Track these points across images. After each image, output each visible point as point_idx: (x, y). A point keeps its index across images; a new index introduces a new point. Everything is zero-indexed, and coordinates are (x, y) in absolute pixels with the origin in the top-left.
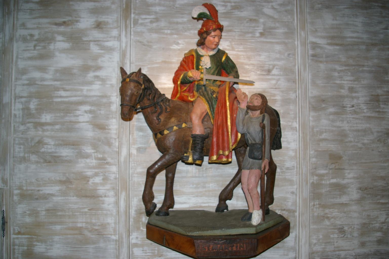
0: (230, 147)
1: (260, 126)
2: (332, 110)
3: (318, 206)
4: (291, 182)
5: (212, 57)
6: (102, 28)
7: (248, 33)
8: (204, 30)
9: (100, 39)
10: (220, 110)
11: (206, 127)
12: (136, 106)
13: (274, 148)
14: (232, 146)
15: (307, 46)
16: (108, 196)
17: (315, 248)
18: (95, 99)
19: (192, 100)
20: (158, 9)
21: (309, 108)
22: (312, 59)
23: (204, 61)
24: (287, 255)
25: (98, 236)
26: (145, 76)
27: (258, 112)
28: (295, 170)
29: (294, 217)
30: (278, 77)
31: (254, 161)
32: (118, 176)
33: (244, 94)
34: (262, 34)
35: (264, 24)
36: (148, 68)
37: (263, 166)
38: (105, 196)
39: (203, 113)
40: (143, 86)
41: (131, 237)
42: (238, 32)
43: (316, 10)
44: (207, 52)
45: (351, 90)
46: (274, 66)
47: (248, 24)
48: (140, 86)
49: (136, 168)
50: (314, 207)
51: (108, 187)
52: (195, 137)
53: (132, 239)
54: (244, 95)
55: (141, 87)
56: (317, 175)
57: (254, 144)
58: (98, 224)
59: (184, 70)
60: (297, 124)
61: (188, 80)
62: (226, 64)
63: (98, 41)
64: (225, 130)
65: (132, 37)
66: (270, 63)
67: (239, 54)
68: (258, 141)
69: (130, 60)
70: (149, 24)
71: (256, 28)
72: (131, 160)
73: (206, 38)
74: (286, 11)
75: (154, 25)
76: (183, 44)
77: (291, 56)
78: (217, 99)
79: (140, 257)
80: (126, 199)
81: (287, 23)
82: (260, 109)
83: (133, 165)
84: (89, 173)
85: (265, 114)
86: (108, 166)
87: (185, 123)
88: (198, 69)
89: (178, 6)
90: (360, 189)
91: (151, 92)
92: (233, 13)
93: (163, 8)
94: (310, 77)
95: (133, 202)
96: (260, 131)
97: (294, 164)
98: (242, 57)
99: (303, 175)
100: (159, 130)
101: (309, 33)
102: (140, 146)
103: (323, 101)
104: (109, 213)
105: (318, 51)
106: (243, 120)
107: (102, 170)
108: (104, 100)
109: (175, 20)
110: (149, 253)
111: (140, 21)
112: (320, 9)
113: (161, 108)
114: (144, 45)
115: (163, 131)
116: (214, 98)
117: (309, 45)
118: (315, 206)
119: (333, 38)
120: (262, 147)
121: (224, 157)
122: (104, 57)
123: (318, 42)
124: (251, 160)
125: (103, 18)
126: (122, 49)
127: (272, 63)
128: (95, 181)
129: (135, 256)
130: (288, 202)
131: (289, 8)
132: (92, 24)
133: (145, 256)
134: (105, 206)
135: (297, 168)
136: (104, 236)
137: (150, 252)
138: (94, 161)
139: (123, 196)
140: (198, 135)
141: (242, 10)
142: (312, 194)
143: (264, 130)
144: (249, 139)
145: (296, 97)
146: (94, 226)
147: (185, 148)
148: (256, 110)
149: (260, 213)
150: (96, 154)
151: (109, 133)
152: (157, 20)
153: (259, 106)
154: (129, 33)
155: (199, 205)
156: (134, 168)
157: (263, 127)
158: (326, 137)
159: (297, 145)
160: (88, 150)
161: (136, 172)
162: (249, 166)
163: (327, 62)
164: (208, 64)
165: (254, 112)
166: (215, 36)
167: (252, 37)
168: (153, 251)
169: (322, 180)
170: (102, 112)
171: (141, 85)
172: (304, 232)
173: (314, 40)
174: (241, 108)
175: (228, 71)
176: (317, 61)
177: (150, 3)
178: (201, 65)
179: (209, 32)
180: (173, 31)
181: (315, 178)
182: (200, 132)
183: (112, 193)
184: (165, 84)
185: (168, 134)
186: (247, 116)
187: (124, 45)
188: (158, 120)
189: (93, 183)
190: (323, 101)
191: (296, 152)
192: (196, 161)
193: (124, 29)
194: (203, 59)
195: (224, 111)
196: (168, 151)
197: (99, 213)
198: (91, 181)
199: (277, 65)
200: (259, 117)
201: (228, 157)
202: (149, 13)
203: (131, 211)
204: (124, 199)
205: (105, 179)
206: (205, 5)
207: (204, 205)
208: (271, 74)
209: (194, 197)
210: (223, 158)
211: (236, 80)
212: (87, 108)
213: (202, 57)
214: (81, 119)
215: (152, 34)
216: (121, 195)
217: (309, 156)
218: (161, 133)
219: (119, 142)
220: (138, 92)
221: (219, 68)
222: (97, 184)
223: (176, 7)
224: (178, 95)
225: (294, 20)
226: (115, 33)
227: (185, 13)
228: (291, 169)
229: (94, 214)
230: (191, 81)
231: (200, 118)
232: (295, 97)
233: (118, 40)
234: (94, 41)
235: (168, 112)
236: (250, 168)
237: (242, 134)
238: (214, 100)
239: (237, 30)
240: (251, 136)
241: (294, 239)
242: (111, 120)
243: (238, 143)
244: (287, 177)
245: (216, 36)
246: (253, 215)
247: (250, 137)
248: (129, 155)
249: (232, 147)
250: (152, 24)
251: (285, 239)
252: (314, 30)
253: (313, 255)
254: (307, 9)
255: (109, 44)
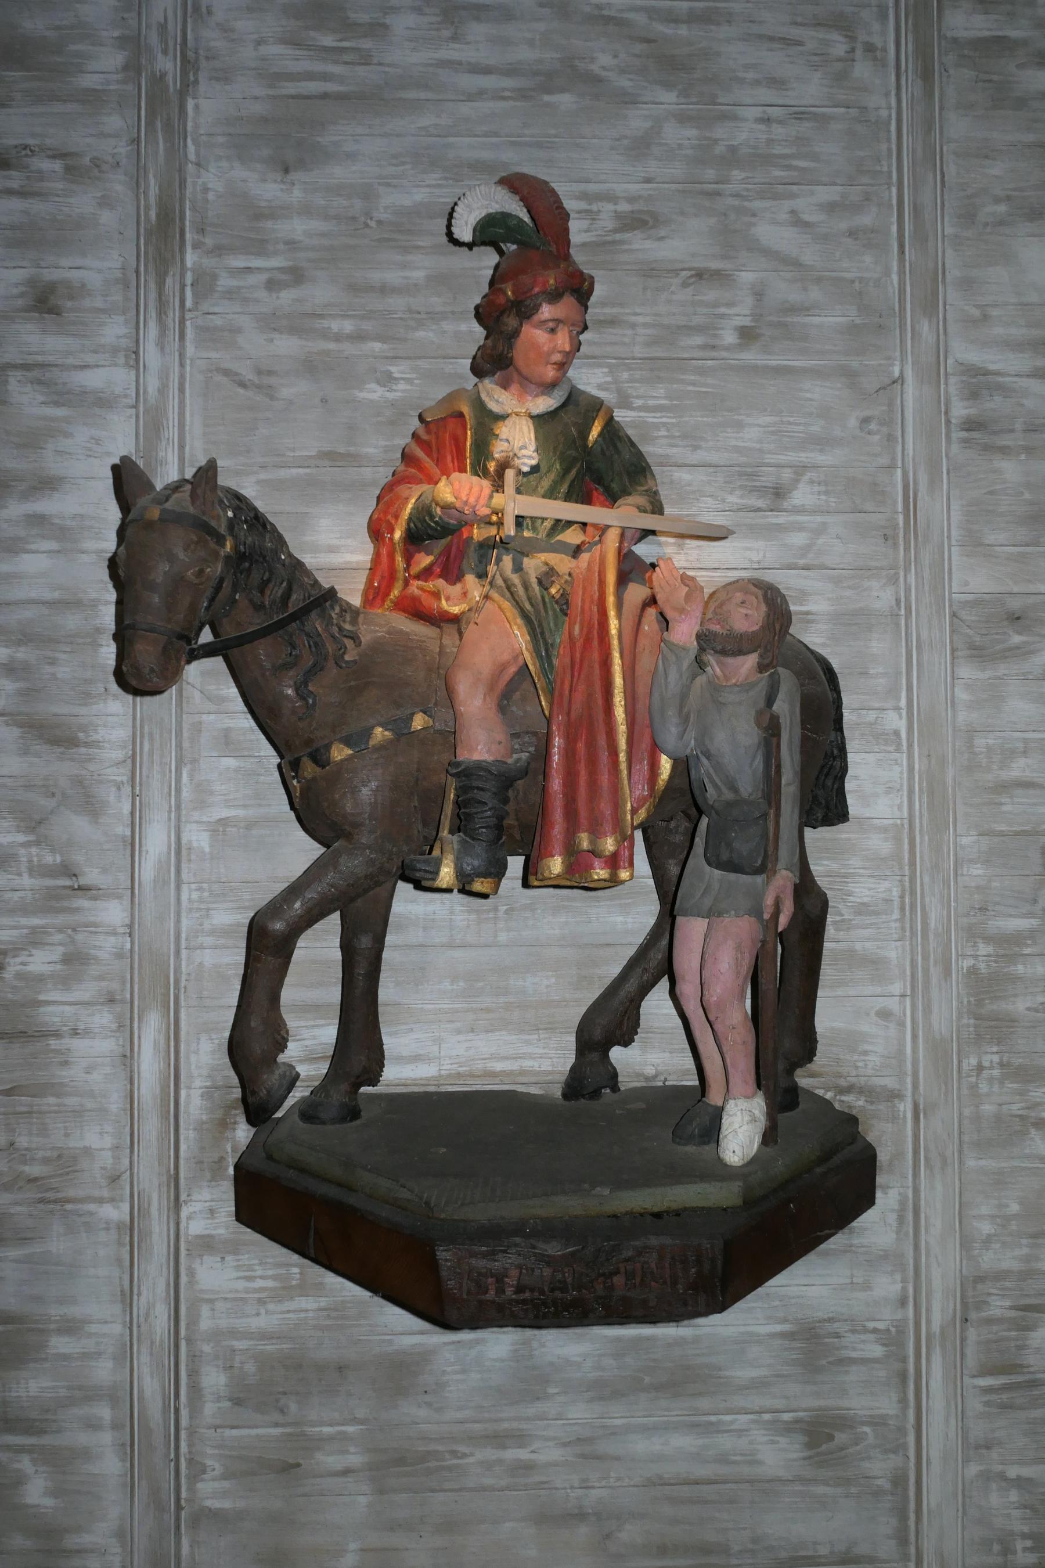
0: (625, 815)
1: (758, 724)
3: (996, 1072)
4: (875, 964)
5: (540, 420)
6: (55, 311)
7: (690, 329)
8: (505, 294)
9: (51, 359)
10: (578, 655)
11: (518, 729)
13: (816, 820)
14: (634, 811)
15: (946, 384)
16: (88, 1033)
17: (988, 1260)
18: (28, 613)
19: (455, 610)
20: (298, 227)
21: (953, 650)
22: (966, 441)
23: (508, 441)
24: (867, 1287)
25: (41, 1206)
26: (239, 500)
27: (750, 661)
28: (896, 915)
29: (894, 1118)
30: (819, 519)
31: (732, 876)
32: (128, 946)
33: (690, 583)
34: (747, 335)
35: (759, 294)
36: (258, 482)
37: (769, 901)
38: (75, 1033)
39: (503, 667)
40: (228, 546)
41: (185, 1212)
42: (645, 325)
43: (986, 224)
44: (521, 399)
46: (800, 470)
47: (690, 290)
48: (212, 545)
49: (208, 909)
50: (978, 1075)
51: (86, 991)
53: (189, 1218)
54: (688, 586)
55: (217, 547)
56: (988, 939)
57: (730, 804)
58: (40, 1154)
59: (419, 482)
60: (901, 718)
61: (436, 523)
62: (608, 453)
63: (42, 366)
64: (602, 741)
65: (190, 350)
66: (781, 458)
67: (651, 420)
68: (750, 790)
69: (182, 447)
70: (262, 294)
71: (723, 310)
72: (184, 876)
73: (516, 333)
74: (852, 233)
75: (286, 297)
76: (409, 381)
77: (873, 426)
78: (567, 603)
79: (226, 1299)
80: (162, 1041)
81: (857, 285)
82: (759, 647)
83: (195, 896)
85: (780, 670)
86: (86, 903)
87: (425, 713)
88: (480, 469)
89: (383, 216)
91: (271, 573)
92: (626, 247)
93: (318, 225)
94: (956, 516)
95: (193, 1058)
96: (760, 743)
97: (890, 890)
98: (663, 433)
99: (931, 937)
100: (309, 742)
101: (952, 328)
102: (225, 813)
103: (1015, 619)
104: (89, 1104)
105: (995, 404)
106: (684, 697)
107: (60, 920)
109: (376, 277)
110: (262, 1277)
111: (225, 282)
112: (1001, 223)
113: (316, 644)
114: (242, 385)
115: (328, 747)
116: (551, 602)
117: (952, 380)
118: (985, 1073)
120: (765, 816)
121: (597, 863)
122: (68, 435)
123: (992, 367)
124: (717, 873)
126: (145, 400)
127: (792, 457)
128: (30, 968)
129: (202, 1291)
130: (866, 1053)
131: (866, 219)
132: (15, 291)
133: (247, 1291)
134: (74, 1074)
135: (902, 909)
136: (69, 1207)
137: (270, 1273)
138: (26, 881)
140: (479, 766)
141: (663, 233)
142: (972, 1021)
143: (774, 740)
144: (706, 781)
145: (898, 602)
146: (25, 1163)
147: (425, 824)
148: (740, 652)
149: (757, 1112)
150: (34, 850)
151: (90, 759)
152: (296, 276)
153: (753, 632)
154: (173, 335)
155: (479, 1066)
156: (199, 910)
157: (771, 729)
158: (1027, 774)
159: (900, 807)
161: (207, 926)
162: (708, 902)
163: (1029, 450)
164: (524, 452)
165: (730, 660)
166: (558, 321)
167: (705, 347)
168: (283, 1271)
169: (1011, 959)
170: (63, 672)
171: (220, 540)
172: (939, 1187)
173: (974, 356)
174: (673, 644)
175: (614, 486)
176: (987, 448)
177: (263, 204)
178: (493, 459)
179: (528, 302)
180: (367, 326)
181: (984, 949)
182: (489, 751)
183: (103, 1019)
184: (332, 550)
185: (349, 759)
186: (701, 680)
187: (152, 384)
188: (303, 698)
189: (20, 976)
190: (1015, 619)
191: (898, 840)
192: (473, 880)
193: (153, 313)
194: (504, 430)
195: (596, 656)
196: (348, 836)
197: (48, 1105)
198: (13, 966)
199: (815, 467)
200: (752, 685)
201: (613, 862)
202: (260, 247)
203: (188, 1096)
204: (156, 1043)
206: (514, 183)
207: (499, 1066)
208: (786, 505)
209: (459, 1032)
210: (591, 867)
211: (648, 521)
213: (500, 424)
215: (276, 336)
216: (139, 1028)
217: (956, 855)
218: (319, 758)
219: (134, 796)
220: (201, 572)
221: (574, 472)
222: (40, 979)
223: (380, 222)
224: (395, 593)
225: (887, 273)
227: (418, 247)
228: (877, 913)
229: (23, 1109)
230: (449, 524)
231: (491, 688)
232: (894, 603)
233: (127, 365)
234: (26, 367)
235: (347, 662)
236: (710, 909)
237: (676, 763)
238: (554, 610)
239: (640, 319)
240: (718, 767)
241: (892, 1218)
242: (100, 707)
243: (661, 799)
244: (858, 946)
245: (561, 326)
246: (726, 1121)
247: (711, 771)
248: (178, 852)
249: (632, 818)
250: (274, 295)
251: (854, 1224)
252: (976, 313)
253: (979, 1286)
254: (946, 219)
255: (93, 379)
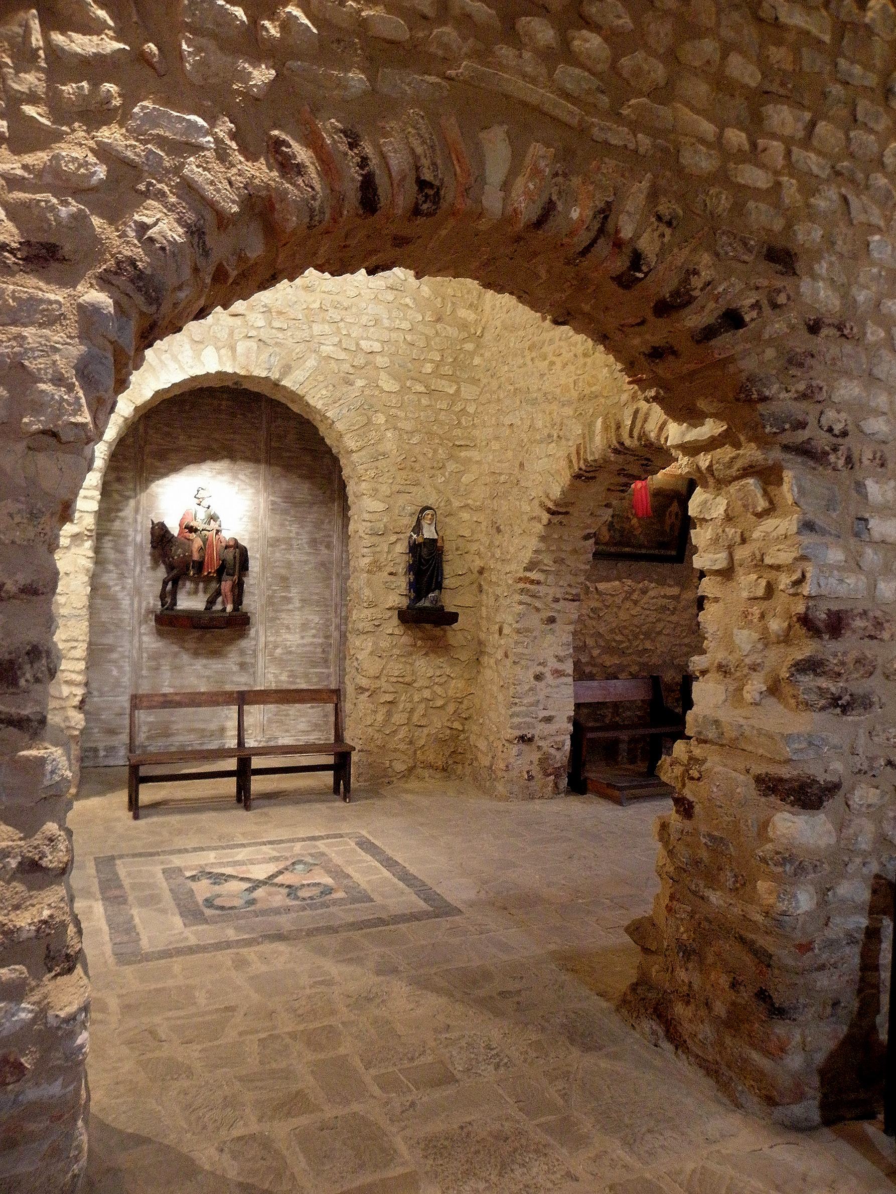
2: (283, 547)
12: (790, 627)
45: (297, 533)
52: (194, 562)
84: (111, 583)
90: (302, 600)
103: (278, 540)
108: (123, 533)
119: (286, 497)
125: (122, 475)
134: (123, 606)
139: (136, 600)
160: (111, 567)
183: (128, 598)
205: (123, 588)
212: (110, 538)
214: (105, 545)
226: (131, 486)
